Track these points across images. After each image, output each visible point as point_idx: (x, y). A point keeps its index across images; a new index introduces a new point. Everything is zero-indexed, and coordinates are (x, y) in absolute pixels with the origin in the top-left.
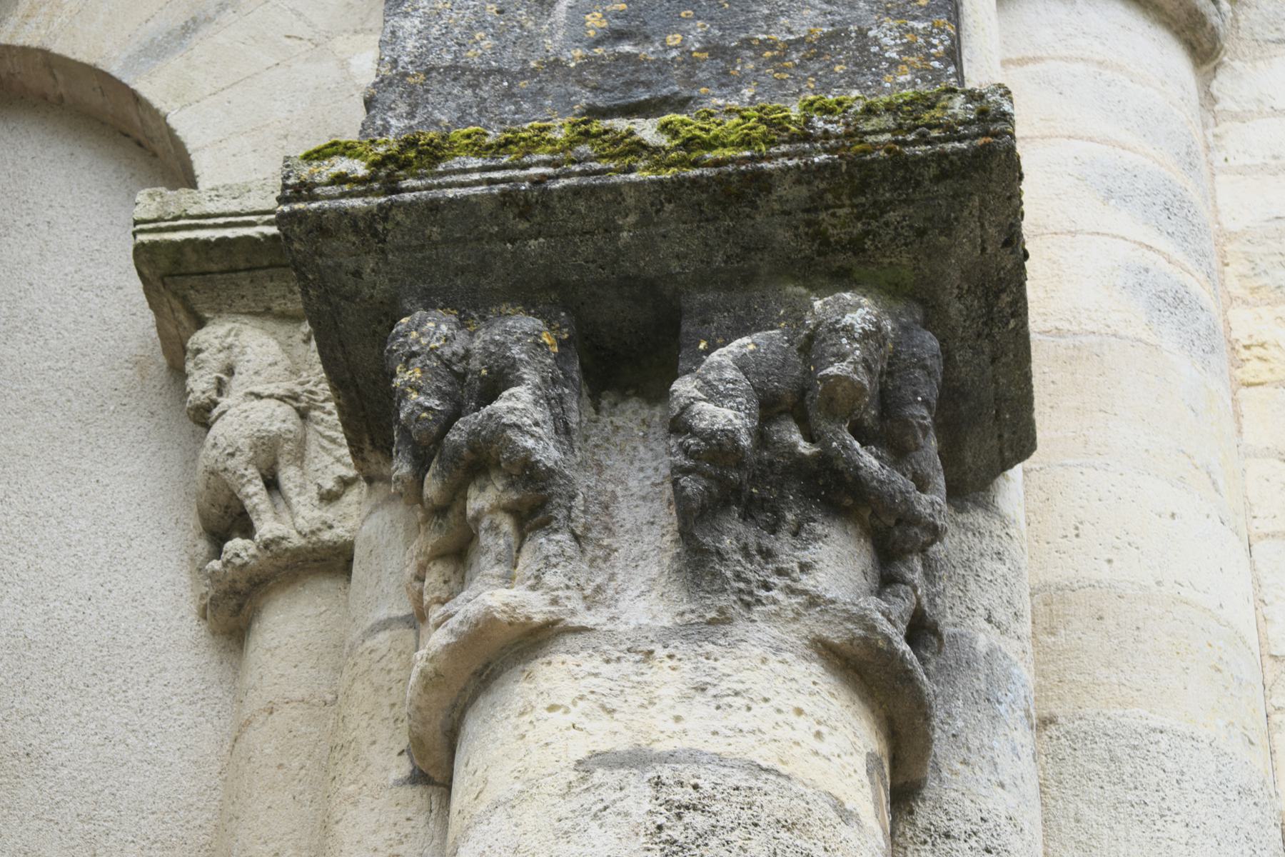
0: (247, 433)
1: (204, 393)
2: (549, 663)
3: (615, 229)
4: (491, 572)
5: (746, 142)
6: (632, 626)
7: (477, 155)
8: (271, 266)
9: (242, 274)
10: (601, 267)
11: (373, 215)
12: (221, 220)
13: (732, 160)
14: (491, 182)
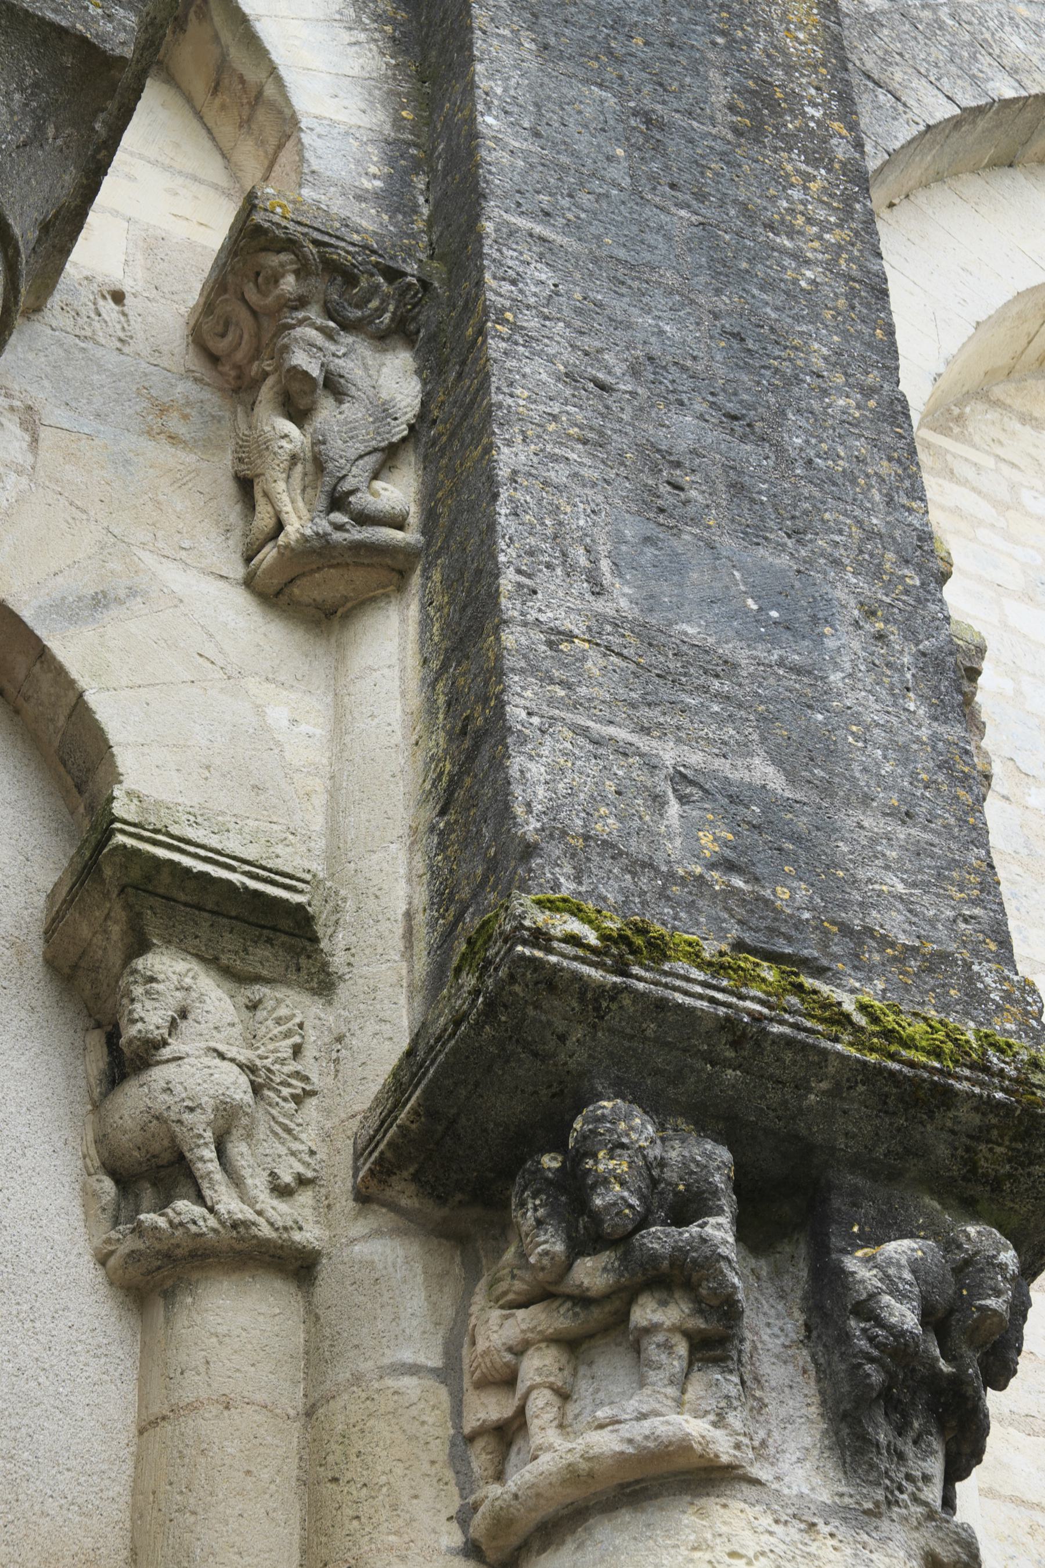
0: (212, 1092)
1: (158, 1028)
2: (725, 1506)
3: (805, 1089)
4: (663, 1390)
5: (936, 1053)
6: (794, 1492)
7: (699, 967)
8: (236, 918)
9: (205, 915)
10: (778, 1117)
11: (604, 991)
12: (202, 853)
13: (925, 1067)
14: (712, 1000)
